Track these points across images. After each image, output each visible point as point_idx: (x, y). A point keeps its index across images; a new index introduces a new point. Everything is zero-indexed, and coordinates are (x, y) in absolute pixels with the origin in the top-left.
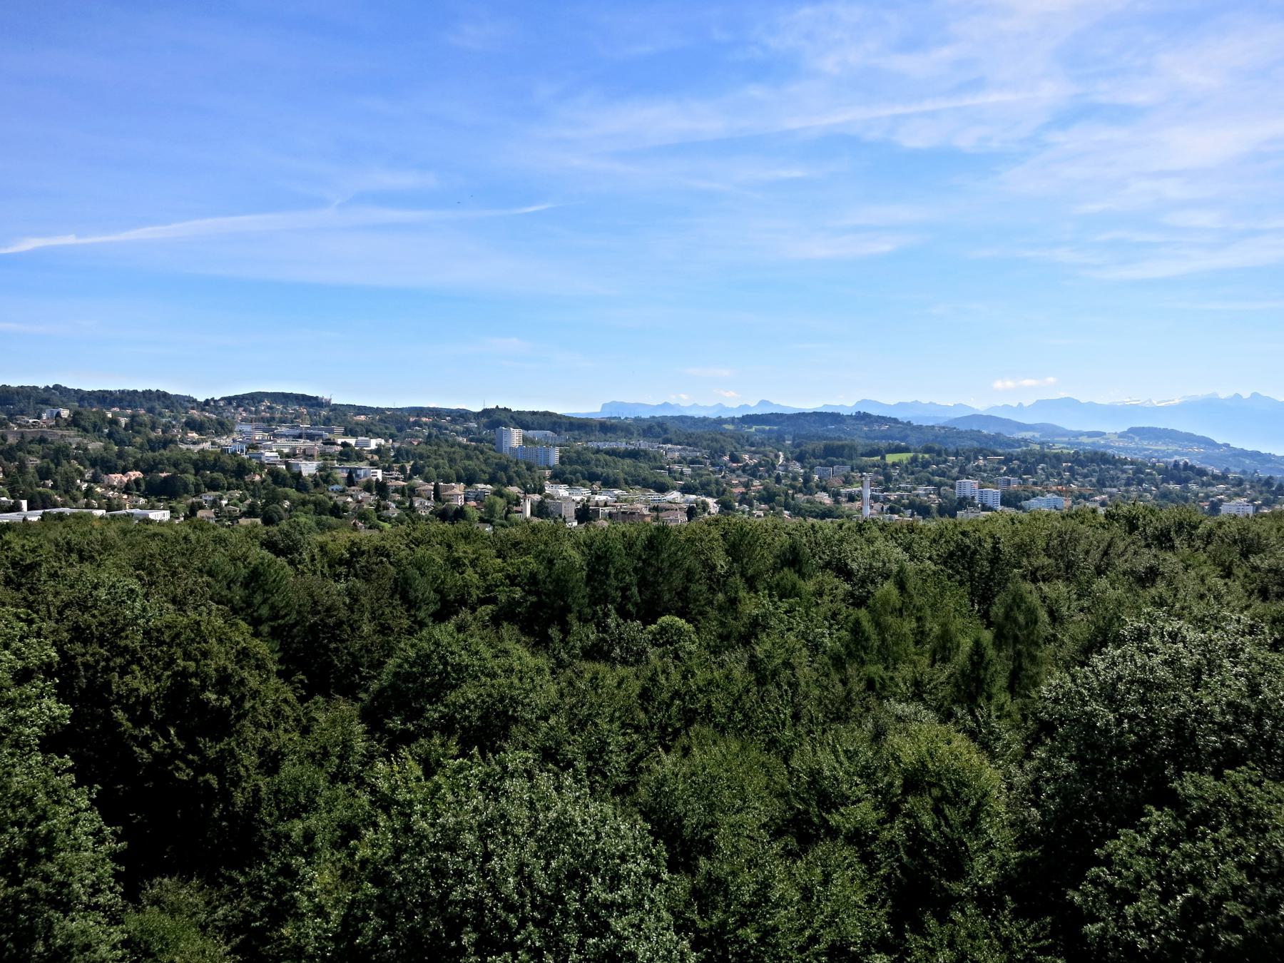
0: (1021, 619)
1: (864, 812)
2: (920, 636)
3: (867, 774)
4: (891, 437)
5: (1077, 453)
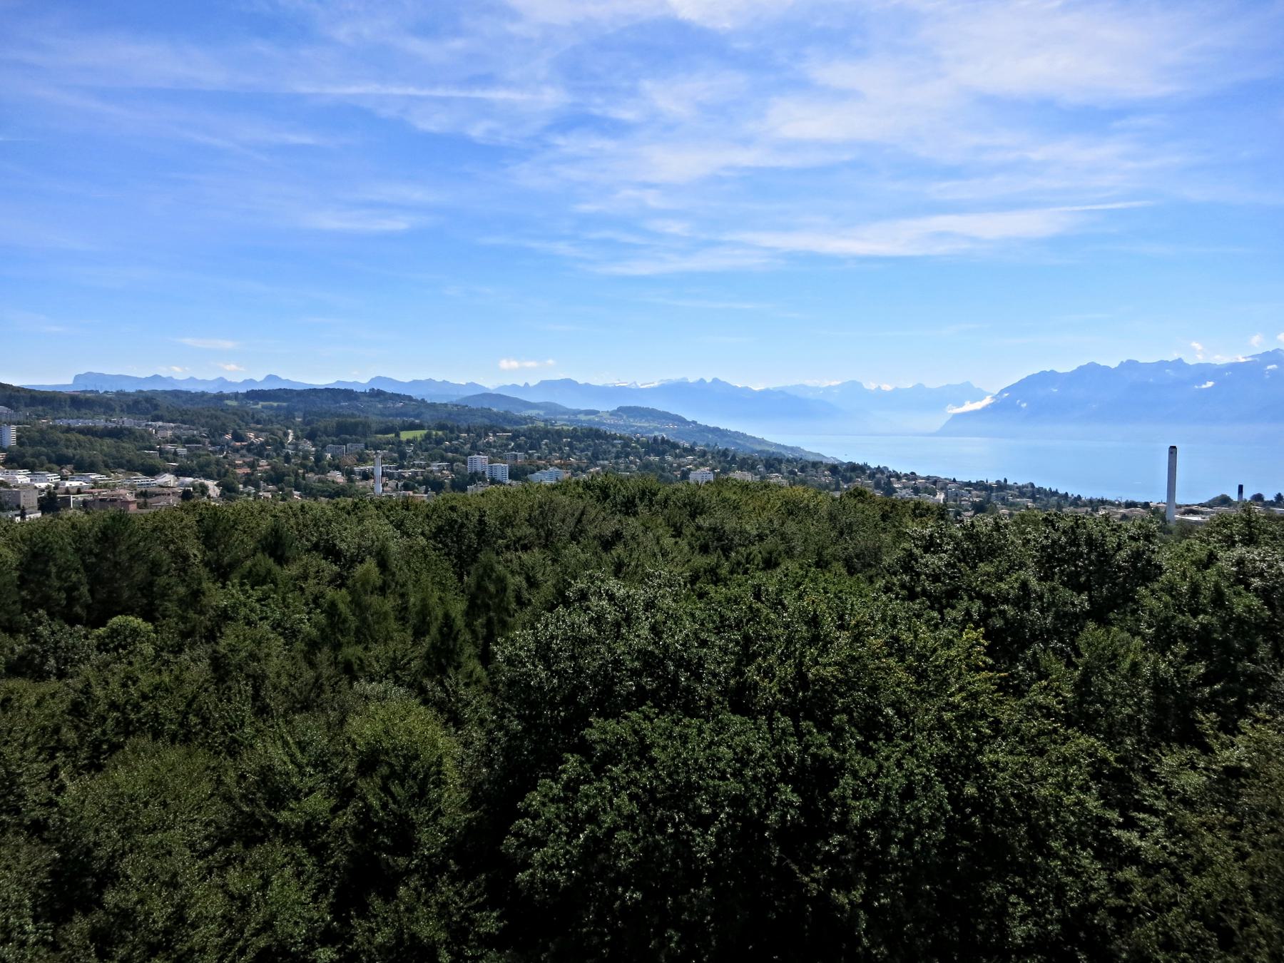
0: (492, 588)
1: (318, 803)
2: (402, 613)
3: (322, 764)
4: (406, 415)
5: (575, 429)
